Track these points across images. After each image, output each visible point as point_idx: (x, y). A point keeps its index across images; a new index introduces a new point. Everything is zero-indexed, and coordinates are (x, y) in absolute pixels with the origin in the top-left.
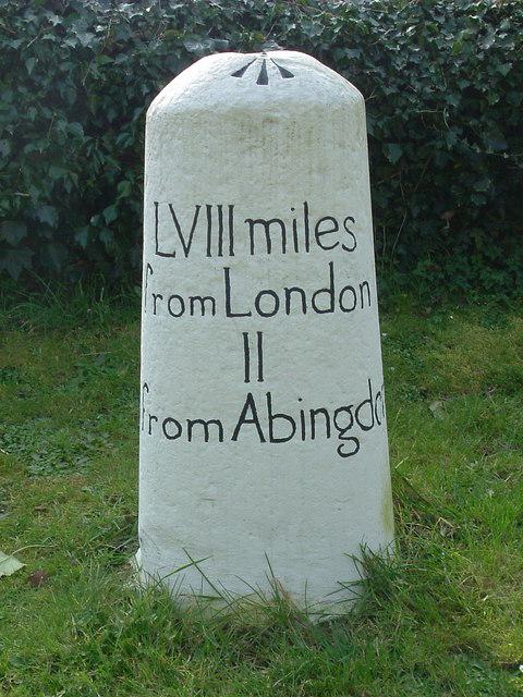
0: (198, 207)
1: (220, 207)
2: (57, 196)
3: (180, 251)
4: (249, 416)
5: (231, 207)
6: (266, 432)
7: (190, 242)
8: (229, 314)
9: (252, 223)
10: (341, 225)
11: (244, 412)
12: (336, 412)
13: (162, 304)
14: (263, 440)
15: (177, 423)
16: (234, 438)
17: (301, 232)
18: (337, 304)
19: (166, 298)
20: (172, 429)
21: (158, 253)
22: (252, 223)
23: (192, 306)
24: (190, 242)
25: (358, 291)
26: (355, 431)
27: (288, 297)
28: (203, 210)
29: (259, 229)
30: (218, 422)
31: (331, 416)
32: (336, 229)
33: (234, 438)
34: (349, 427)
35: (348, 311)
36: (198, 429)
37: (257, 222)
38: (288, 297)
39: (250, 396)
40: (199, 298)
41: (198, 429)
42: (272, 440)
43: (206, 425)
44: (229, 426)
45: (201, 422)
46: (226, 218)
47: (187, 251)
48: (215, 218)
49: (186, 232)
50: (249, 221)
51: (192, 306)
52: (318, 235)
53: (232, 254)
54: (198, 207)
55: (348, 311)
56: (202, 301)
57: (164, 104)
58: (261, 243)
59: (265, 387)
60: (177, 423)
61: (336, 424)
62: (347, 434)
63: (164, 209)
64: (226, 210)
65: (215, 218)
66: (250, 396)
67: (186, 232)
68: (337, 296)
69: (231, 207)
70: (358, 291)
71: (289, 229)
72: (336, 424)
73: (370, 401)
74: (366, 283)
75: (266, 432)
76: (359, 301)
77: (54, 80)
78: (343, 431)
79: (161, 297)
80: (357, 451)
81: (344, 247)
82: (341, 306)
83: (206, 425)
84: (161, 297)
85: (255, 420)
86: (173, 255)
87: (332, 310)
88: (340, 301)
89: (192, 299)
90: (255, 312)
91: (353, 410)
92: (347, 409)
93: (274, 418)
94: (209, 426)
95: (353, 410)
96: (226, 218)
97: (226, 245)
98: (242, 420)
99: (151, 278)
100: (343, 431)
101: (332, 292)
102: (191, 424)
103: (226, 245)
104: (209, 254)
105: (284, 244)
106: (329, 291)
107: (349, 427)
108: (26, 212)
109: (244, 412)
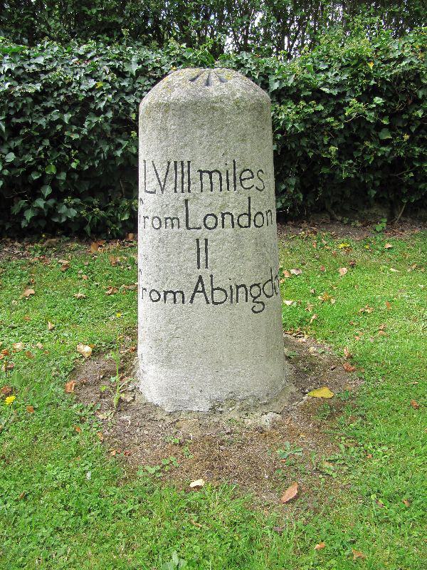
0: (169, 163)
4: (200, 288)
7: (164, 186)
10: (255, 174)
13: (149, 222)
14: (208, 303)
15: (158, 293)
17: (231, 178)
23: (166, 223)
24: (164, 186)
25: (265, 215)
26: (263, 298)
27: (223, 218)
34: (259, 296)
36: (170, 296)
38: (223, 218)
41: (170, 296)
43: (174, 294)
46: (185, 170)
50: (199, 171)
51: (166, 223)
52: (241, 180)
53: (189, 191)
55: (259, 227)
58: (207, 186)
62: (257, 300)
68: (252, 218)
69: (189, 162)
71: (224, 177)
78: (255, 298)
85: (203, 291)
86: (154, 193)
89: (167, 219)
90: (203, 227)
92: (258, 285)
95: (261, 286)
97: (186, 186)
98: (196, 291)
100: (255, 298)
102: (166, 293)
103: (186, 186)
104: (176, 191)
105: (221, 185)
107: (259, 296)
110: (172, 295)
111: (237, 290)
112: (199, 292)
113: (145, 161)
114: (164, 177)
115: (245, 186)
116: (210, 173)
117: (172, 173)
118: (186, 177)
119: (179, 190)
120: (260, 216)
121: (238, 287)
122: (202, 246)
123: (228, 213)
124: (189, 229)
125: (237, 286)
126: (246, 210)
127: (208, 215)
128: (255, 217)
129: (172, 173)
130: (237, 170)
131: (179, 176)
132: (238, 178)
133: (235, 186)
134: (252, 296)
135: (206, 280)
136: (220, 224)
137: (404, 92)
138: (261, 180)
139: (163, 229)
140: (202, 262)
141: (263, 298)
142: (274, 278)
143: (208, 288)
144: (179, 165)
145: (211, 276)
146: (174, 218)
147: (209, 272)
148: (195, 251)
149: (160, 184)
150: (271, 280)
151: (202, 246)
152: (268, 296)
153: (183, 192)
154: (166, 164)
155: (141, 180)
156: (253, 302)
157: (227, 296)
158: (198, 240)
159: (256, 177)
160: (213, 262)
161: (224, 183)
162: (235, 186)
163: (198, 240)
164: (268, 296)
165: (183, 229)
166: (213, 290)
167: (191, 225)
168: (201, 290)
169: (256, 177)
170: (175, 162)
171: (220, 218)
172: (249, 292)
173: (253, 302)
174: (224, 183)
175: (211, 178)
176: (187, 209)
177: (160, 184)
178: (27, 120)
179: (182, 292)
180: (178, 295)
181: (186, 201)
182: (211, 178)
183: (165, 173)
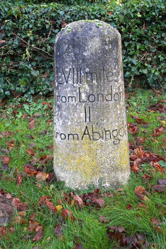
2: (109, 41)
6: (91, 138)
11: (85, 131)
30: (77, 134)
36: (71, 137)
41: (71, 137)
42: (93, 140)
45: (71, 134)
60: (64, 135)
61: (66, 99)
62: (116, 138)
68: (113, 96)
72: (66, 99)
75: (91, 138)
77: (36, 7)
87: (112, 100)
88: (114, 97)
91: (118, 130)
98: (84, 134)
100: (115, 137)
101: (111, 95)
102: (69, 135)
106: (110, 94)
108: (68, 37)
109: (85, 131)
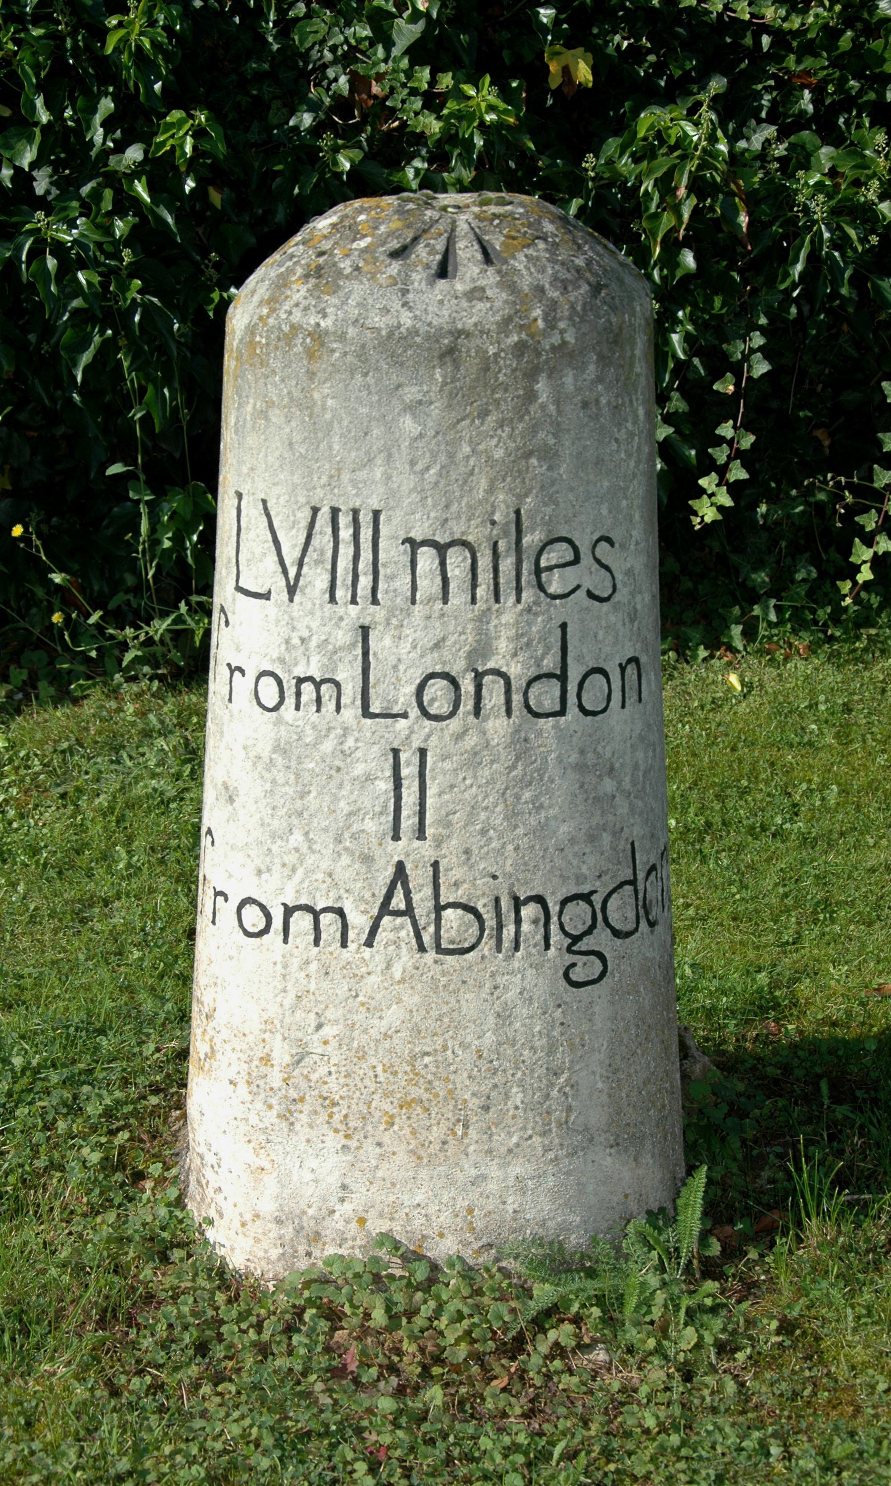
0: (315, 511)
1: (356, 512)
3: (279, 585)
4: (398, 902)
5: (376, 514)
7: (298, 575)
8: (366, 713)
9: (414, 545)
10: (584, 550)
12: (564, 903)
13: (243, 685)
14: (422, 948)
15: (263, 907)
16: (369, 943)
17: (507, 565)
18: (572, 699)
19: (251, 675)
20: (253, 918)
21: (239, 589)
22: (414, 545)
23: (298, 694)
24: (298, 575)
25: (615, 677)
26: (601, 940)
27: (479, 688)
28: (324, 515)
29: (427, 559)
31: (554, 909)
32: (576, 561)
33: (369, 943)
34: (589, 931)
35: (594, 714)
36: (302, 922)
37: (424, 543)
38: (479, 688)
39: (400, 867)
40: (310, 679)
41: (302, 922)
43: (316, 915)
44: (359, 921)
46: (366, 534)
47: (292, 590)
48: (346, 533)
49: (291, 555)
50: (409, 540)
51: (298, 694)
52: (538, 571)
53: (375, 601)
54: (315, 511)
55: (594, 714)
56: (318, 685)
57: (238, 334)
58: (429, 585)
59: (397, 850)
60: (263, 907)
62: (582, 946)
63: (252, 513)
64: (365, 518)
65: (346, 533)
66: (400, 867)
67: (291, 555)
68: (572, 687)
69: (376, 514)
70: (615, 677)
71: (484, 562)
73: (633, 882)
74: (634, 660)
75: (427, 938)
76: (616, 696)
78: (576, 939)
79: (243, 672)
80: (260, 704)
81: (590, 595)
82: (527, 706)
83: (316, 915)
84: (243, 672)
85: (409, 911)
86: (266, 596)
89: (300, 681)
90: (414, 712)
91: (597, 899)
92: (586, 897)
93: (445, 907)
94: (487, 679)
95: (597, 899)
96: (366, 534)
97: (365, 581)
98: (385, 909)
99: (224, 629)
100: (576, 939)
101: (563, 678)
102: (289, 911)
103: (365, 581)
104: (332, 599)
105: (474, 586)
107: (589, 931)
110: (309, 918)
111: (517, 912)
112: (397, 913)
113: (240, 496)
114: (297, 554)
115: (552, 590)
116: (442, 549)
117: (323, 539)
118: (366, 555)
119: (341, 593)
120: (599, 678)
121: (518, 904)
122: (409, 771)
123: (497, 672)
124: (366, 713)
125: (516, 899)
126: (550, 663)
127: (432, 676)
128: (581, 685)
129: (323, 539)
130: (526, 540)
131: (346, 552)
132: (527, 567)
133: (519, 590)
134: (567, 934)
135: (419, 878)
136: (467, 705)
137: (601, 1389)
138: (607, 568)
139: (288, 709)
140: (408, 822)
141: (601, 940)
142: (641, 875)
143: (422, 899)
144: (344, 520)
145: (435, 865)
146: (324, 681)
147: (426, 850)
148: (385, 785)
149: (285, 572)
150: (633, 882)
151: (409, 771)
152: (616, 933)
153: (354, 601)
154: (307, 513)
155: (224, 550)
156: (569, 950)
157: (482, 929)
158: (396, 752)
159: (586, 559)
160: (445, 822)
161: (485, 576)
162: (519, 590)
163: (396, 752)
164: (616, 933)
165: (351, 713)
166: (439, 908)
167: (375, 708)
168: (403, 906)
169: (586, 559)
170: (356, 512)
171: (467, 685)
172: (554, 919)
173: (569, 950)
174: (485, 576)
175: (443, 564)
176: (366, 654)
177: (285, 572)
178: (639, 321)
179: (340, 912)
180: (326, 919)
181: (365, 631)
182: (443, 564)
183: (302, 539)
